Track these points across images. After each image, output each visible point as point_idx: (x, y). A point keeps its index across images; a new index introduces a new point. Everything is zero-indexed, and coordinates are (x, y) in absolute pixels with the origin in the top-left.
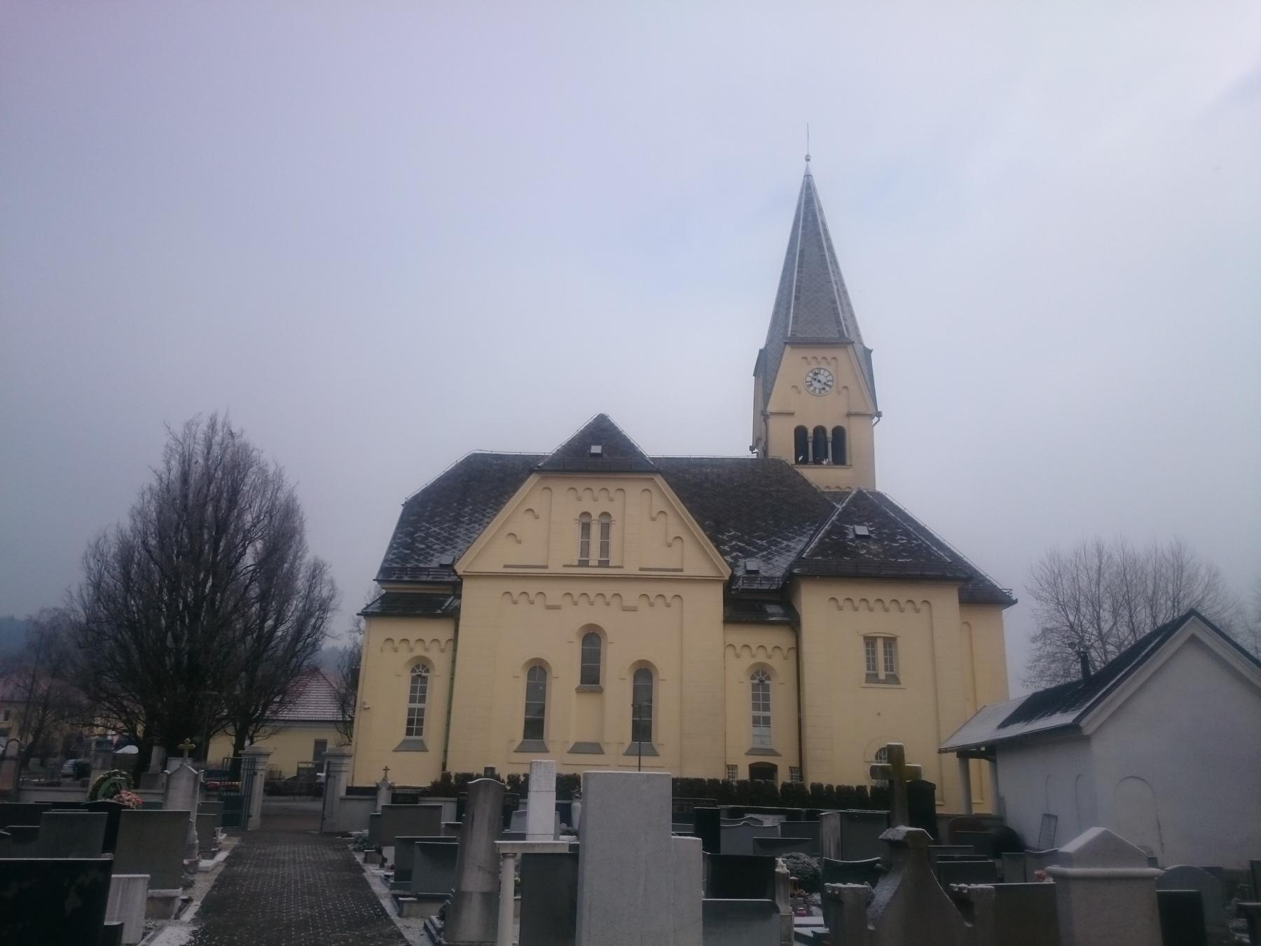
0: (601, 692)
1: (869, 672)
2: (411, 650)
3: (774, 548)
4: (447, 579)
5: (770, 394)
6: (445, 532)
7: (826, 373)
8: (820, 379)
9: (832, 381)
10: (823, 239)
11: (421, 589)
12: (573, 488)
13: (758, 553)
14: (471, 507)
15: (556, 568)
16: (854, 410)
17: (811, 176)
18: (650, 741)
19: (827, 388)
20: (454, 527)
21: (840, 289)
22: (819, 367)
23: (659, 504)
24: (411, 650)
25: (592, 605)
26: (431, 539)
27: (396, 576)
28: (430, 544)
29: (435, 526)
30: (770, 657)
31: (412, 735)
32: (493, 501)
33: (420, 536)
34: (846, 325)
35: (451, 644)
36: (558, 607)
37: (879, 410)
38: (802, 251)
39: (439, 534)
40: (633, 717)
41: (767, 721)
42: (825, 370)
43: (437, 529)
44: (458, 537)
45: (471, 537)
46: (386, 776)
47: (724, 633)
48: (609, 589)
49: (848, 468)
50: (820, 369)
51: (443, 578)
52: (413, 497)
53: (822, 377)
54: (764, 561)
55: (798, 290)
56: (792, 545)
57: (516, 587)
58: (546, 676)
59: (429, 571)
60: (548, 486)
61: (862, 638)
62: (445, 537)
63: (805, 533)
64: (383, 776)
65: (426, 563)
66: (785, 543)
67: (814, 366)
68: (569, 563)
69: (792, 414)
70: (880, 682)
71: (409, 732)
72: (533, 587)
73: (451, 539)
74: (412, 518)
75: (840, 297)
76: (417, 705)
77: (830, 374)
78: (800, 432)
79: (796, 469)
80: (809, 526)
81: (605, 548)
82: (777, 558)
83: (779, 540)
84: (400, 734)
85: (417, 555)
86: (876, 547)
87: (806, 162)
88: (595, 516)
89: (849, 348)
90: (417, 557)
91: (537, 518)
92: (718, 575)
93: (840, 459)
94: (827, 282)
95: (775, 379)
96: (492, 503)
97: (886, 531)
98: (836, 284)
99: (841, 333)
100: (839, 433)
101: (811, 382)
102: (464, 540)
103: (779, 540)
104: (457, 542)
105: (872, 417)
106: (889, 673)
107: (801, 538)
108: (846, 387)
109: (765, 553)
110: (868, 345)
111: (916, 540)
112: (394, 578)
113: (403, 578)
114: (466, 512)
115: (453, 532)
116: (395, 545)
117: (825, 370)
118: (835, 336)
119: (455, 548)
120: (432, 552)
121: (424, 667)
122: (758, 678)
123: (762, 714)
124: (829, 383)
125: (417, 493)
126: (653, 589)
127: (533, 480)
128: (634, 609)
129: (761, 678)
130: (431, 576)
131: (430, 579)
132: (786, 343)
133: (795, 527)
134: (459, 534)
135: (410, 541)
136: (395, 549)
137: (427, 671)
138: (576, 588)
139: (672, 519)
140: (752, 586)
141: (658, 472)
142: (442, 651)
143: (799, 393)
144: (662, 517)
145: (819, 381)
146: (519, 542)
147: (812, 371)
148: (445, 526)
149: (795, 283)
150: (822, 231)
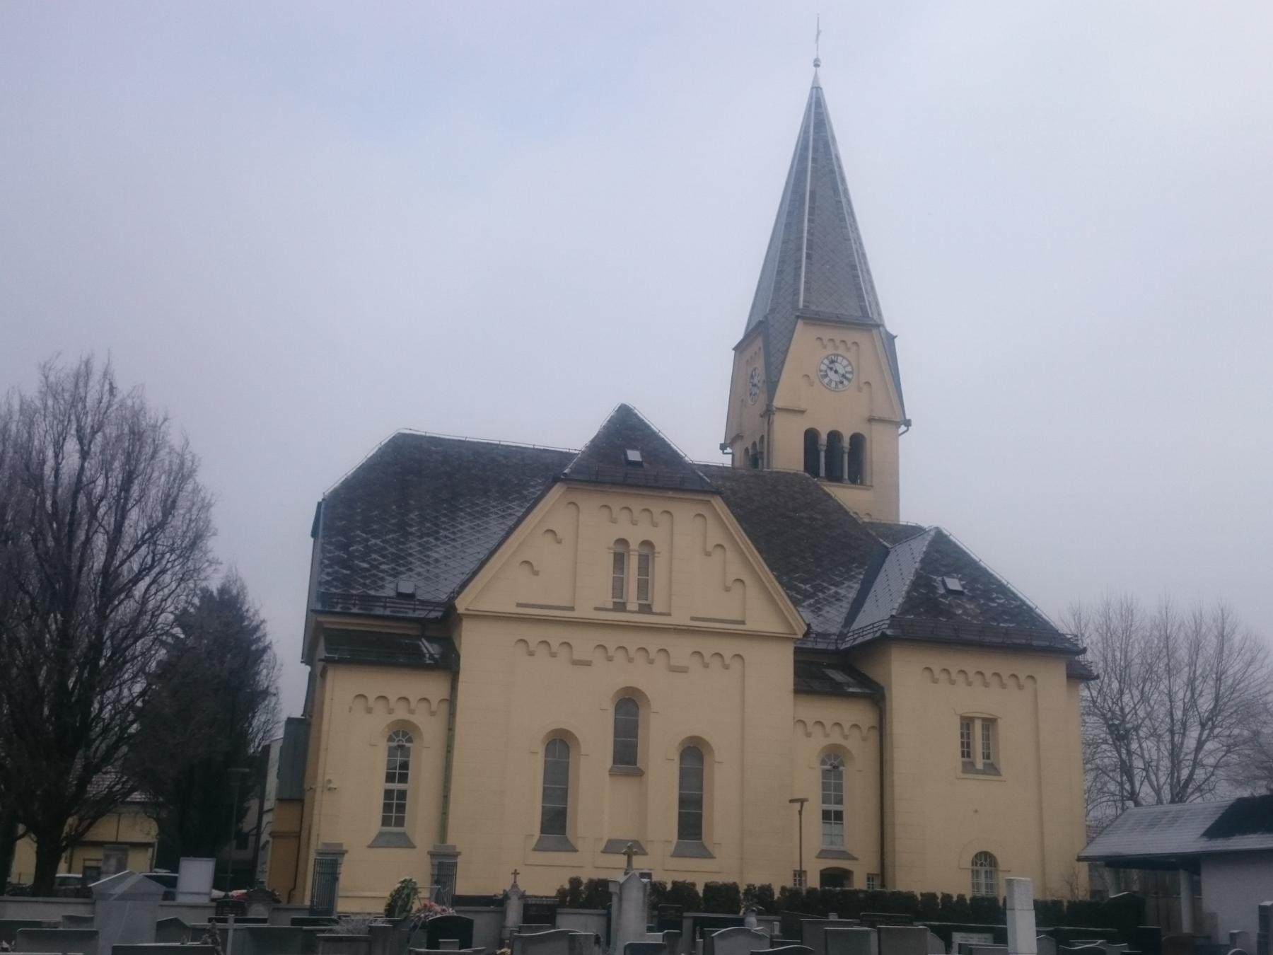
0: (641, 776)
1: (964, 759)
2: (391, 711)
3: (821, 595)
4: (411, 614)
5: (777, 382)
6: (391, 546)
7: (845, 362)
8: (838, 369)
9: (851, 373)
10: (838, 177)
11: (358, 625)
12: (574, 503)
13: (804, 601)
14: (417, 513)
15: (584, 611)
16: (876, 415)
17: (821, 89)
18: (700, 839)
19: (846, 382)
20: (402, 540)
21: (859, 249)
22: (836, 352)
23: (715, 536)
24: (827, 735)
25: (611, 661)
26: (374, 556)
27: (340, 606)
28: (375, 563)
29: (374, 537)
30: (846, 737)
31: (390, 825)
32: (445, 505)
33: (357, 550)
34: (869, 301)
35: (445, 706)
36: (588, 663)
37: (308, 668)
38: (813, 193)
39: (384, 549)
40: (543, 803)
41: (839, 816)
42: (844, 358)
43: (378, 542)
44: (411, 555)
45: (428, 557)
46: (515, 882)
47: (795, 705)
48: (653, 643)
49: (868, 490)
50: (838, 355)
51: (406, 612)
52: (332, 492)
53: (839, 365)
54: (812, 611)
55: (810, 247)
56: (843, 592)
57: (534, 634)
58: (569, 753)
59: (386, 602)
60: (650, 508)
61: (959, 717)
62: (392, 554)
63: (854, 577)
64: (512, 882)
65: (376, 590)
66: (833, 589)
67: (830, 351)
68: (602, 606)
69: (802, 412)
70: (978, 772)
71: (386, 821)
72: (555, 635)
73: (404, 558)
74: (339, 524)
75: (860, 263)
76: (396, 786)
77: (850, 364)
78: (811, 437)
79: (825, 488)
80: (856, 567)
81: (643, 588)
82: (828, 608)
83: (825, 585)
84: (376, 826)
85: (361, 578)
86: (972, 607)
87: (814, 68)
88: (634, 545)
89: (875, 331)
90: (361, 580)
91: (559, 542)
92: (788, 632)
93: (857, 476)
94: (846, 240)
95: (783, 362)
96: (445, 509)
97: (979, 586)
98: (855, 243)
99: (863, 309)
100: (857, 440)
101: (826, 371)
102: (420, 560)
103: (825, 585)
104: (411, 563)
105: (898, 424)
106: (966, 759)
107: (851, 584)
108: (868, 383)
109: (812, 601)
110: (892, 331)
111: (1015, 600)
112: (338, 609)
113: (350, 609)
114: (412, 519)
115: (401, 546)
116: (326, 562)
117: (844, 358)
118: (856, 314)
119: (410, 570)
120: (381, 575)
121: (405, 734)
122: (829, 763)
123: (833, 807)
124: (848, 375)
125: (335, 486)
126: (708, 646)
127: (557, 491)
128: (683, 670)
129: (833, 763)
130: (389, 610)
131: (388, 612)
132: (798, 317)
133: (841, 568)
134: (410, 551)
135: (346, 556)
136: (327, 566)
137: (410, 740)
138: (612, 640)
139: (731, 555)
140: (805, 644)
141: (717, 492)
142: (433, 714)
143: (812, 384)
144: (719, 551)
145: (836, 372)
146: (536, 573)
147: (827, 358)
148: (388, 537)
149: (805, 234)
150: (836, 168)
